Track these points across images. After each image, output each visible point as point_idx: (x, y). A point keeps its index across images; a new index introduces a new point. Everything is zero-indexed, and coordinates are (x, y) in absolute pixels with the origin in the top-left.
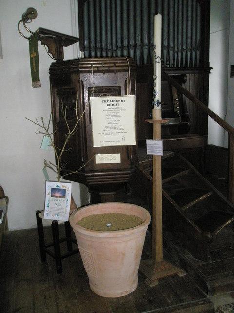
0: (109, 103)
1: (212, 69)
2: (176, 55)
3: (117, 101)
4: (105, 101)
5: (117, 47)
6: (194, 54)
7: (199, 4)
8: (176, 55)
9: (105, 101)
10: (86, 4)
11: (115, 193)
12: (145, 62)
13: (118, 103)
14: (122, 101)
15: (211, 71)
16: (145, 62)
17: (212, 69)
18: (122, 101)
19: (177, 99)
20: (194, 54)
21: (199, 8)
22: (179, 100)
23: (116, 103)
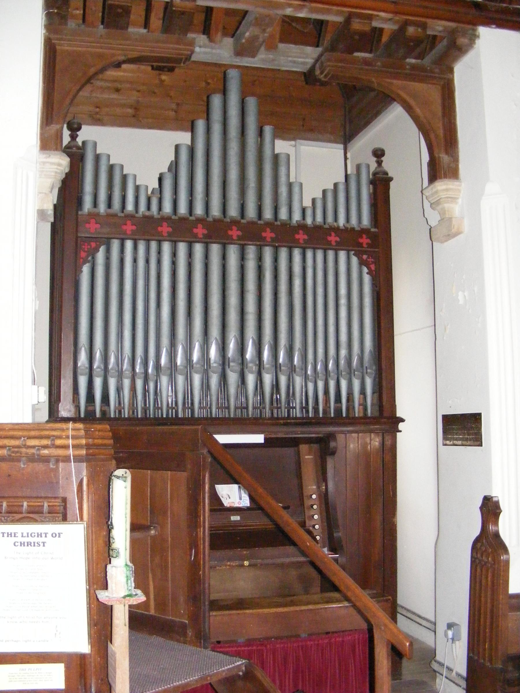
0: (20, 539)
1: (403, 420)
2: (311, 386)
3: (39, 535)
4: (9, 535)
5: (158, 366)
6: (356, 384)
7: (365, 270)
8: (311, 386)
9: (9, 535)
10: (86, 269)
11: (490, 524)
12: (174, 416)
13: (43, 539)
14: (54, 535)
15: (401, 426)
16: (174, 416)
17: (403, 420)
18: (54, 535)
19: (314, 496)
20: (356, 384)
21: (367, 278)
22: (319, 496)
23: (36, 539)
